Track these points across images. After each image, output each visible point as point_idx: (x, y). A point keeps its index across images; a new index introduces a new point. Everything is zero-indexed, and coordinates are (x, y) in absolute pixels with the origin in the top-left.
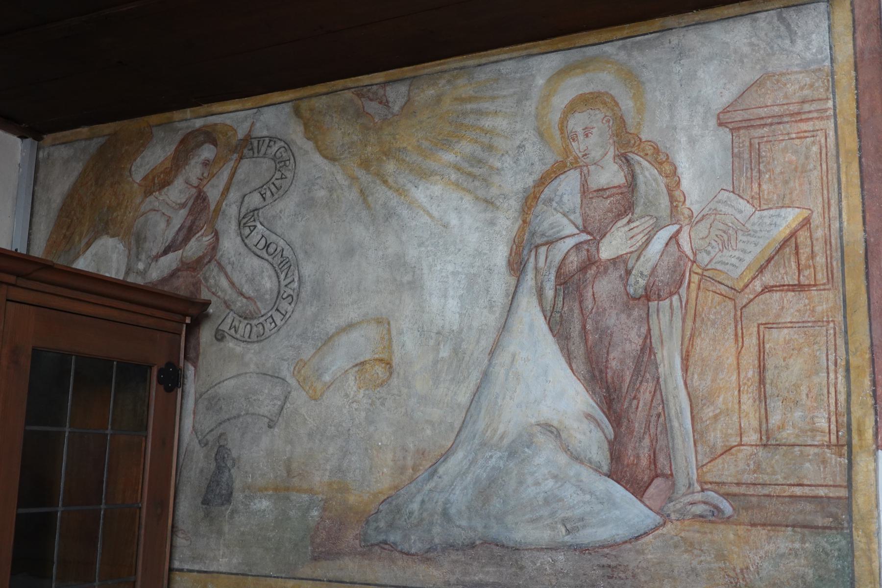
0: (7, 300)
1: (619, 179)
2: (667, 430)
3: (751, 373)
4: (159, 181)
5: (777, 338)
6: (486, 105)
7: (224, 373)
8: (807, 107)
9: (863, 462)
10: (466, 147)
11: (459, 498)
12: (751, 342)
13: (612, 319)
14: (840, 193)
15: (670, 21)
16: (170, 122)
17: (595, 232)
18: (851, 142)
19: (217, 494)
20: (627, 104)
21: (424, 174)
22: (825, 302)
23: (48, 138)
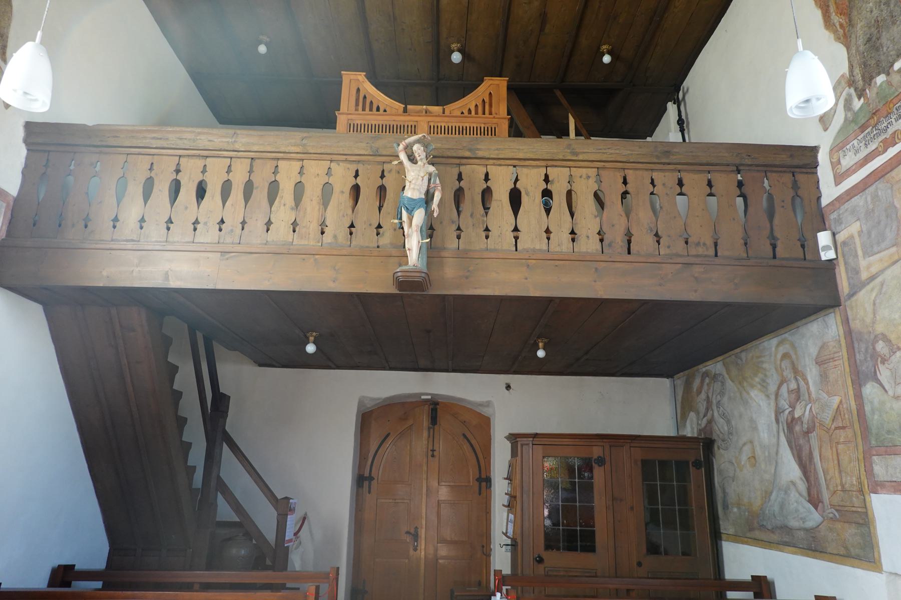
0: (716, 255)
1: (796, 387)
2: (819, 485)
3: (836, 462)
4: (699, 392)
5: (840, 447)
6: (763, 359)
7: (722, 459)
8: (836, 355)
9: (867, 497)
10: (760, 375)
11: (776, 509)
12: (834, 449)
13: (801, 442)
14: (87, 146)
15: (798, 324)
16: (698, 370)
17: (793, 407)
18: (847, 369)
19: (726, 507)
20: (794, 357)
21: (752, 386)
22: (849, 432)
23: (675, 377)
